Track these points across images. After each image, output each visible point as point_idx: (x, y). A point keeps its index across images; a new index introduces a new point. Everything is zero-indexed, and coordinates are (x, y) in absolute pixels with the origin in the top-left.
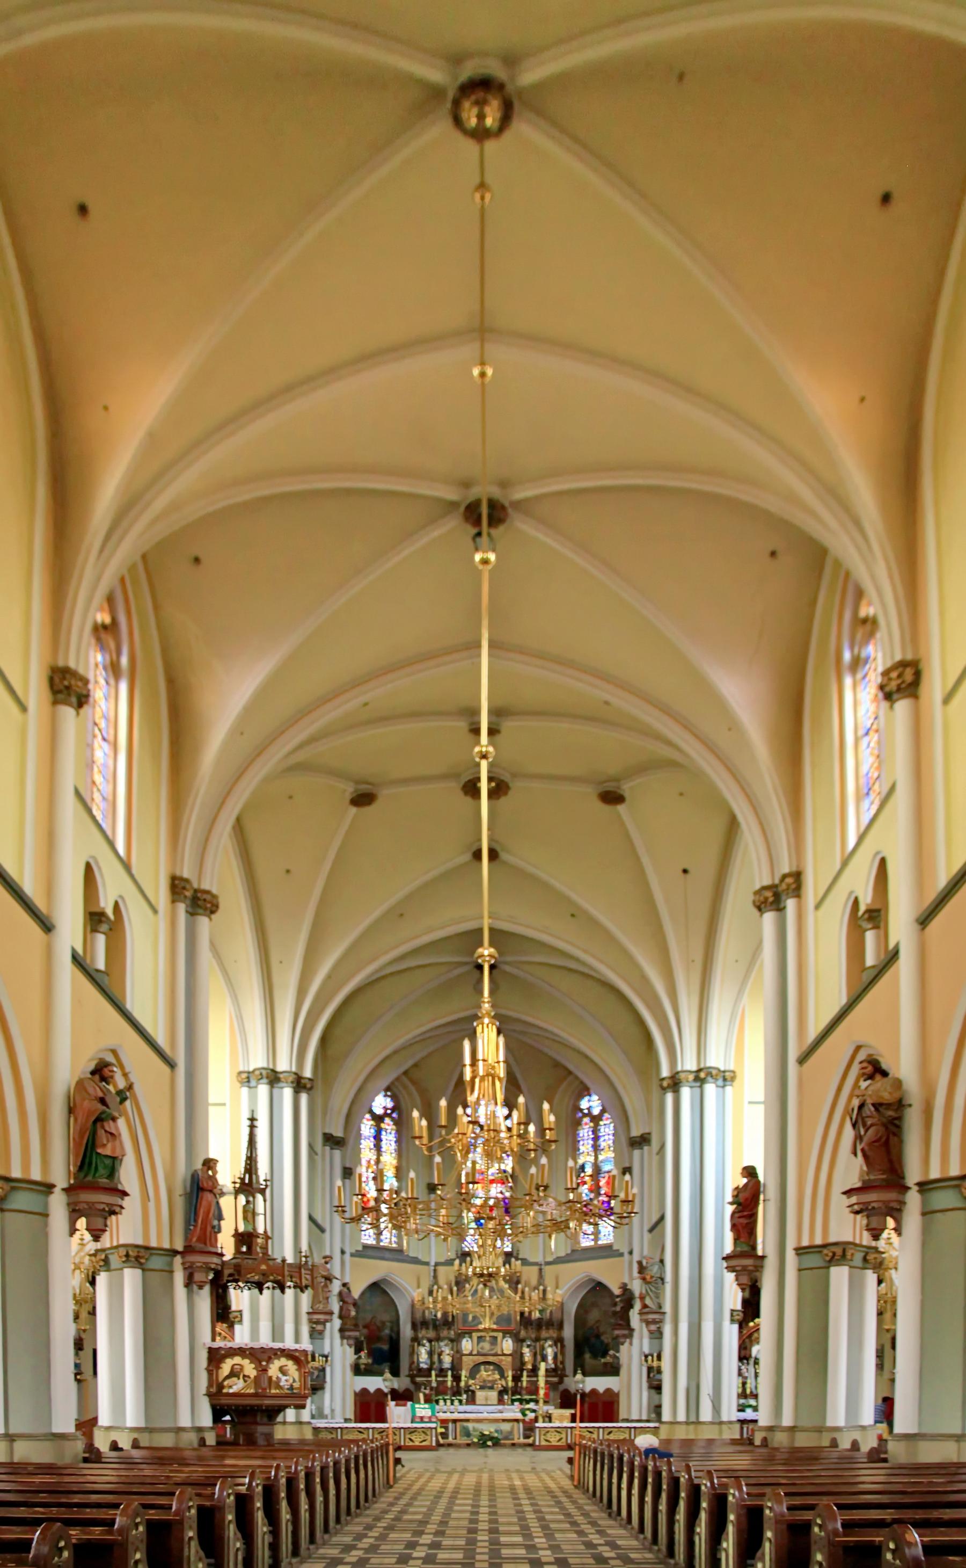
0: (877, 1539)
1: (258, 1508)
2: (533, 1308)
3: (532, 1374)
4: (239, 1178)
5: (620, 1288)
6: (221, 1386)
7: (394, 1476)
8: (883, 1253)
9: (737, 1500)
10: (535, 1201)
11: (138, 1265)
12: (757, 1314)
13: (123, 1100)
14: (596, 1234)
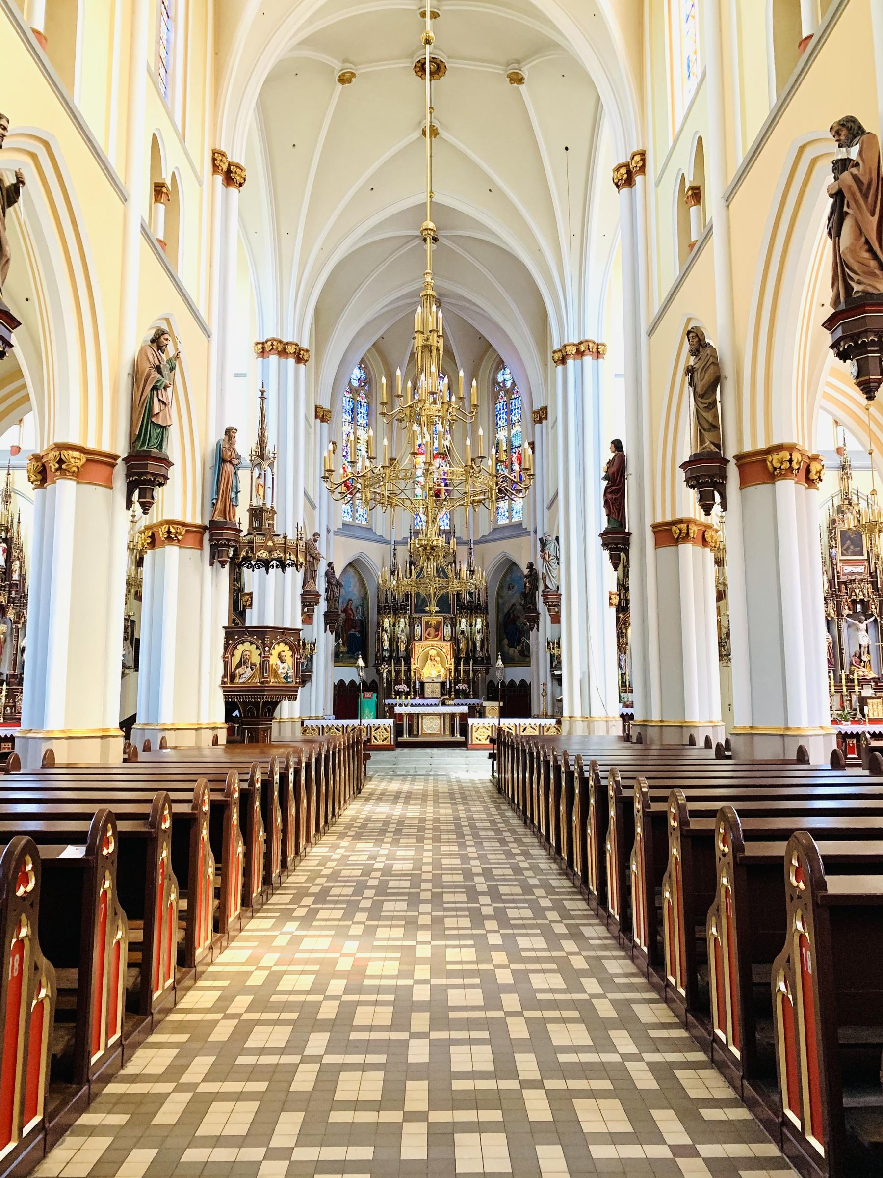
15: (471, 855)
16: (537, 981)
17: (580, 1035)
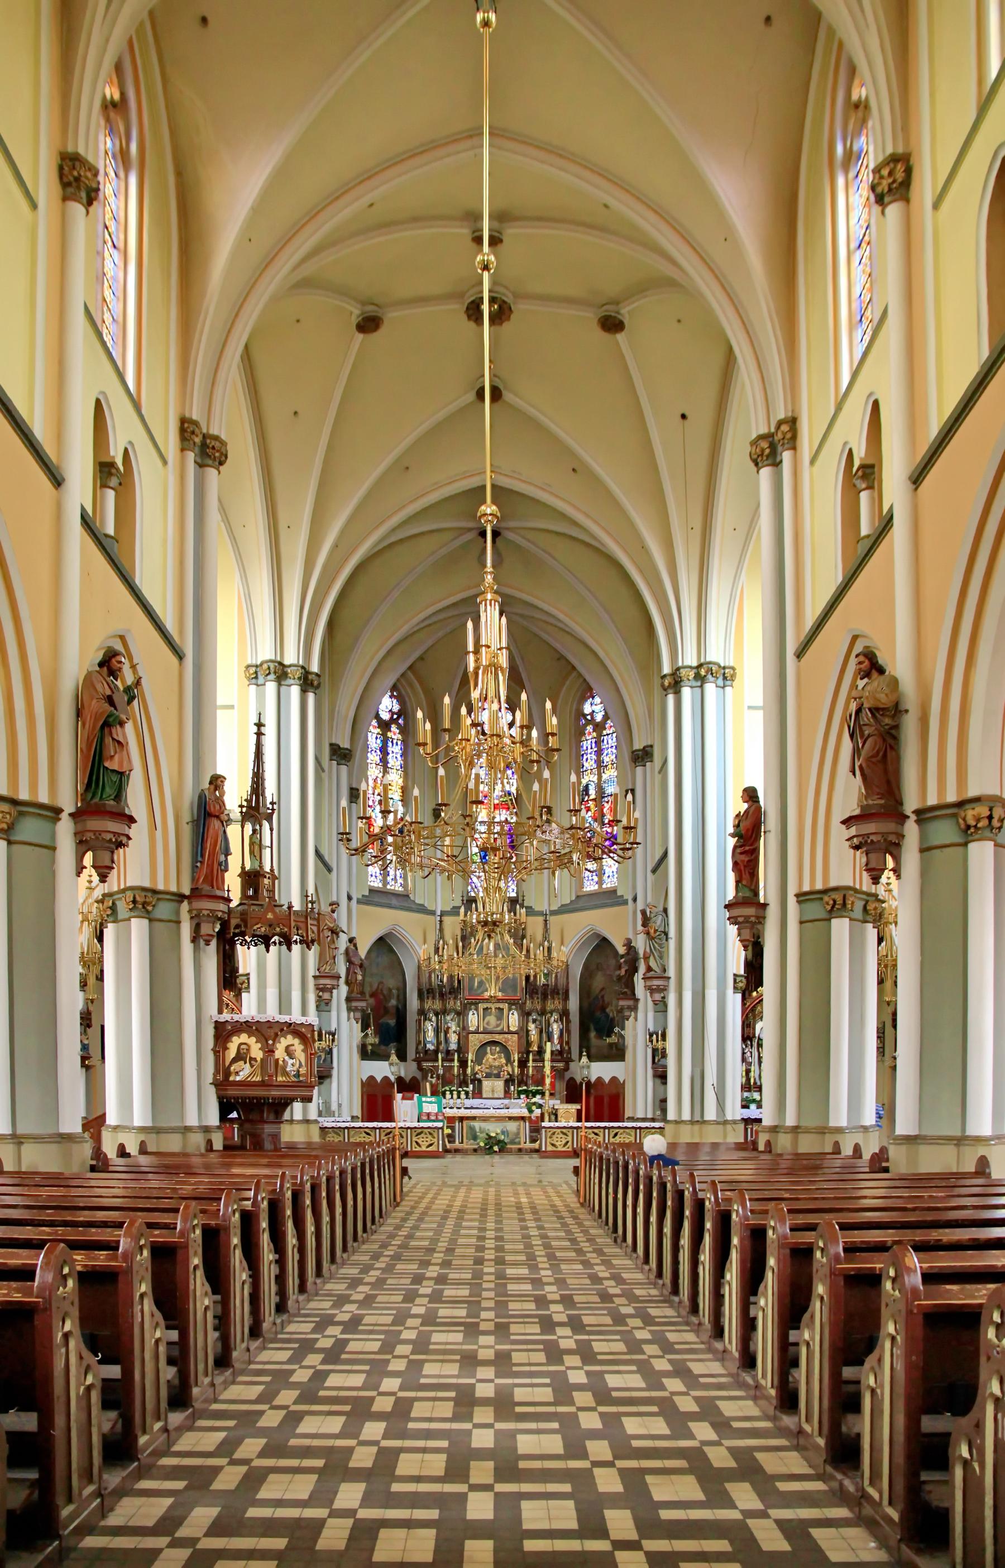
0: (878, 1266)
1: (264, 1230)
2: (538, 970)
3: (537, 1057)
4: (246, 800)
6: (227, 1073)
8: (883, 902)
12: (760, 983)
13: (130, 701)
14: (600, 873)
15: (550, 1297)
16: (632, 1426)
17: (689, 1488)
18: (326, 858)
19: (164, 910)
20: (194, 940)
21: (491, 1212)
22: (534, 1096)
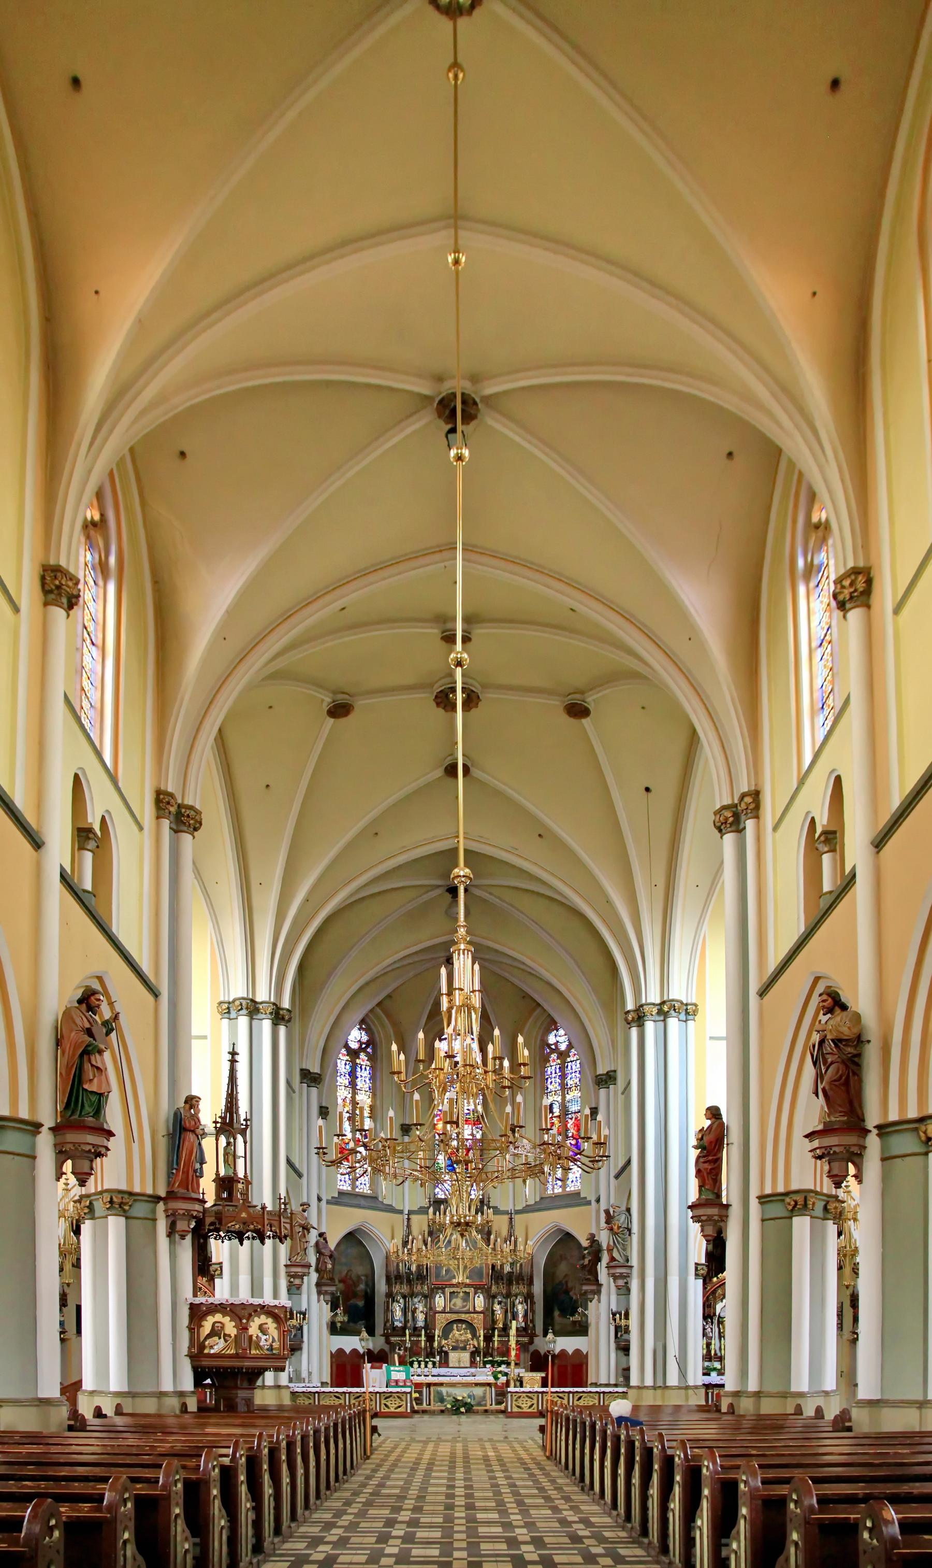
0: (852, 1516)
1: (242, 1482)
2: (504, 1261)
3: (503, 1333)
4: (220, 1117)
5: (587, 1240)
6: (202, 1347)
7: (371, 1445)
8: (843, 1202)
9: (711, 1473)
10: (511, 1143)
11: (122, 1213)
12: (722, 1269)
13: (108, 1033)
15: (520, 1538)
18: (297, 1165)
19: (140, 1209)
20: (170, 1235)
21: (459, 1463)
22: (499, 1366)
